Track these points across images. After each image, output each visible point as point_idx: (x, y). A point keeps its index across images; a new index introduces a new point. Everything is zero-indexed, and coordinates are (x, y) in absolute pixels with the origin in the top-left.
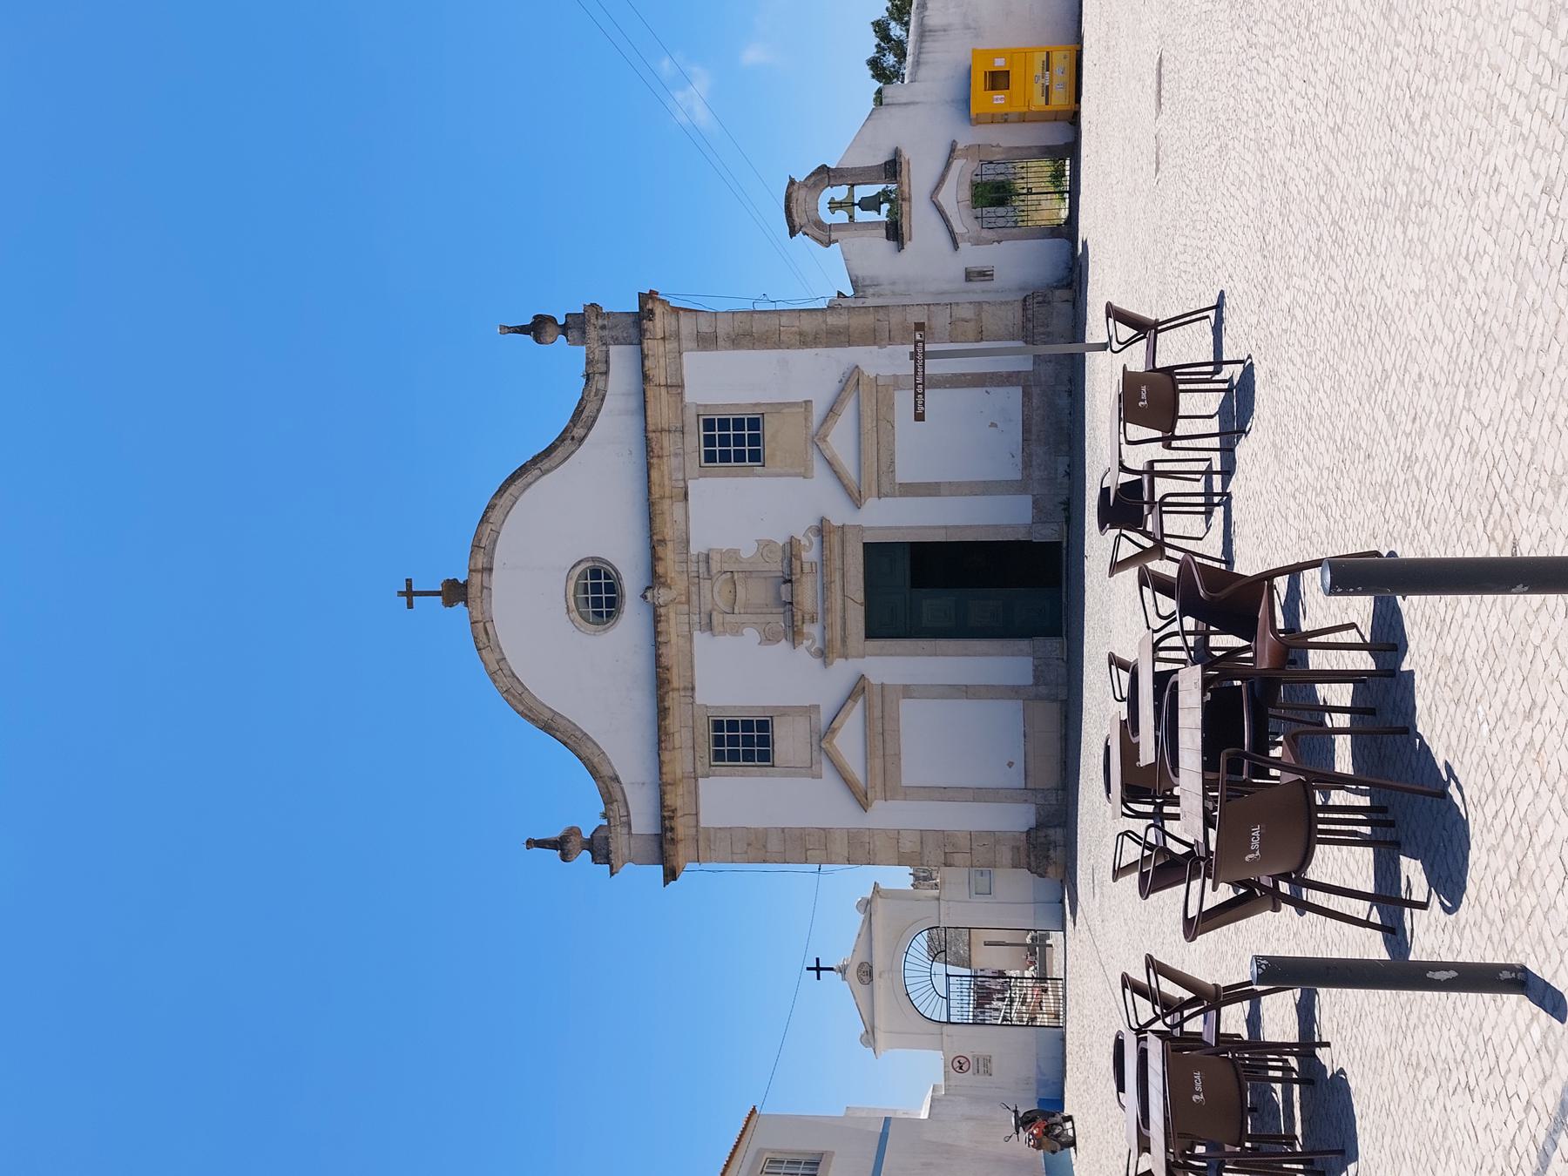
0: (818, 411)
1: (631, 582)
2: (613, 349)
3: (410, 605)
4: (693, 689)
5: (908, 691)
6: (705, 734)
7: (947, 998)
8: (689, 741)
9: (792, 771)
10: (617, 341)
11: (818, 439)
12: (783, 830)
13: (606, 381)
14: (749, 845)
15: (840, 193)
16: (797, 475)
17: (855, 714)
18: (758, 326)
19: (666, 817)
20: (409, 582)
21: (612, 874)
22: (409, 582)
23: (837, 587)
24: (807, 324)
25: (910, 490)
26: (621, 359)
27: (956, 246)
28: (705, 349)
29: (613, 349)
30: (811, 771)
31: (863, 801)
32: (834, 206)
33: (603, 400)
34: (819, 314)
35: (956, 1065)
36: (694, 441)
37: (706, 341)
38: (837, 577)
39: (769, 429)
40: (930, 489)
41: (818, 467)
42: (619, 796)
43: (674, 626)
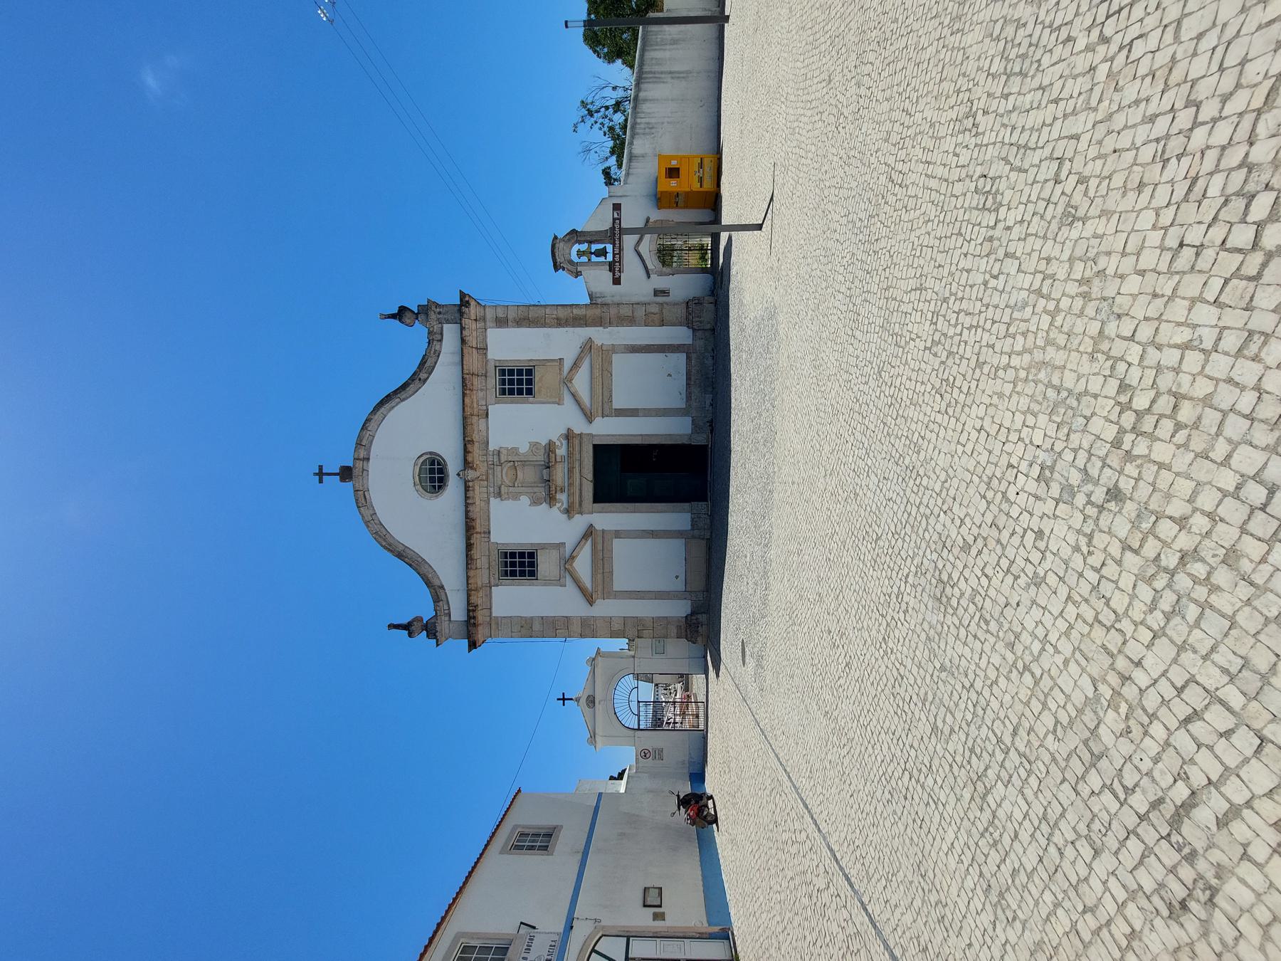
0: (567, 365)
1: (453, 466)
2: (446, 327)
3: (321, 481)
4: (489, 533)
5: (618, 534)
6: (495, 559)
7: (639, 715)
8: (486, 563)
9: (548, 582)
10: (448, 322)
11: (567, 381)
12: (542, 617)
13: (441, 345)
14: (522, 627)
15: (584, 247)
16: (554, 403)
17: (587, 549)
18: (533, 314)
19: (471, 609)
20: (321, 467)
21: (437, 645)
22: (321, 467)
23: (577, 470)
24: (562, 313)
25: (621, 413)
26: (450, 331)
27: (649, 277)
28: (500, 327)
29: (446, 327)
30: (559, 582)
31: (590, 601)
32: (580, 253)
33: (438, 356)
34: (569, 308)
35: (643, 754)
36: (493, 382)
37: (501, 322)
38: (577, 465)
39: (537, 376)
40: (633, 413)
41: (567, 399)
42: (443, 597)
43: (478, 492)
